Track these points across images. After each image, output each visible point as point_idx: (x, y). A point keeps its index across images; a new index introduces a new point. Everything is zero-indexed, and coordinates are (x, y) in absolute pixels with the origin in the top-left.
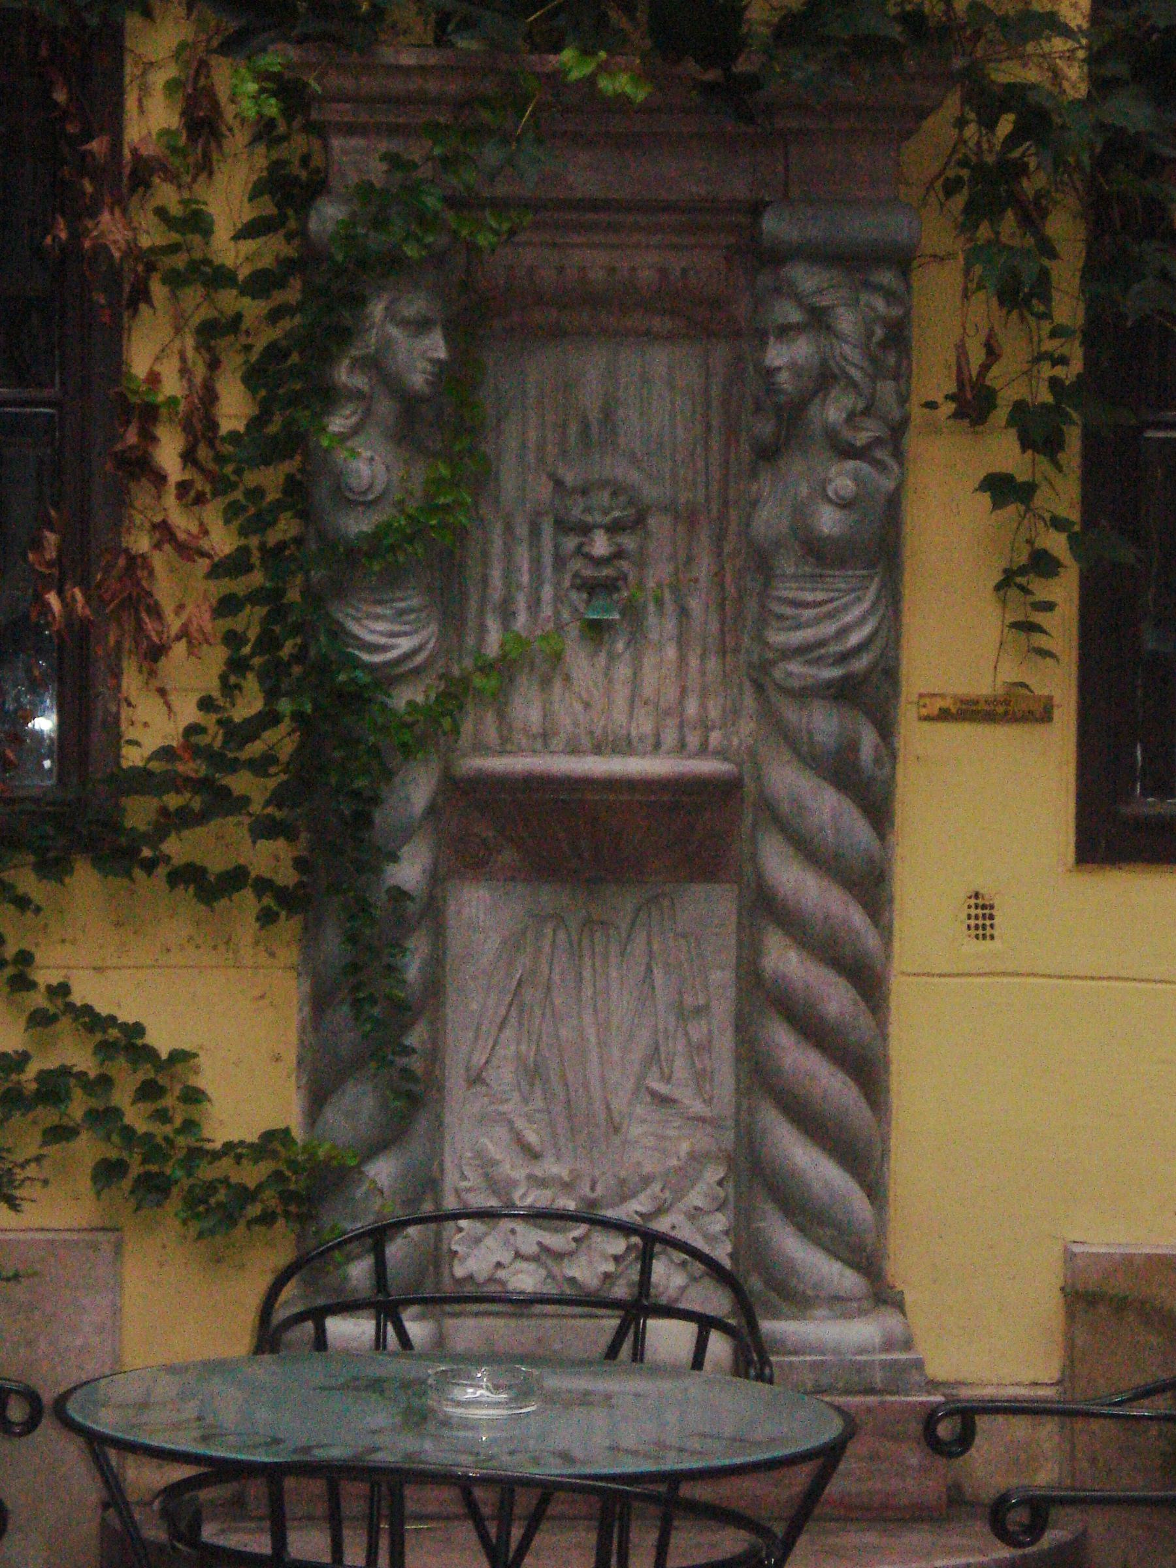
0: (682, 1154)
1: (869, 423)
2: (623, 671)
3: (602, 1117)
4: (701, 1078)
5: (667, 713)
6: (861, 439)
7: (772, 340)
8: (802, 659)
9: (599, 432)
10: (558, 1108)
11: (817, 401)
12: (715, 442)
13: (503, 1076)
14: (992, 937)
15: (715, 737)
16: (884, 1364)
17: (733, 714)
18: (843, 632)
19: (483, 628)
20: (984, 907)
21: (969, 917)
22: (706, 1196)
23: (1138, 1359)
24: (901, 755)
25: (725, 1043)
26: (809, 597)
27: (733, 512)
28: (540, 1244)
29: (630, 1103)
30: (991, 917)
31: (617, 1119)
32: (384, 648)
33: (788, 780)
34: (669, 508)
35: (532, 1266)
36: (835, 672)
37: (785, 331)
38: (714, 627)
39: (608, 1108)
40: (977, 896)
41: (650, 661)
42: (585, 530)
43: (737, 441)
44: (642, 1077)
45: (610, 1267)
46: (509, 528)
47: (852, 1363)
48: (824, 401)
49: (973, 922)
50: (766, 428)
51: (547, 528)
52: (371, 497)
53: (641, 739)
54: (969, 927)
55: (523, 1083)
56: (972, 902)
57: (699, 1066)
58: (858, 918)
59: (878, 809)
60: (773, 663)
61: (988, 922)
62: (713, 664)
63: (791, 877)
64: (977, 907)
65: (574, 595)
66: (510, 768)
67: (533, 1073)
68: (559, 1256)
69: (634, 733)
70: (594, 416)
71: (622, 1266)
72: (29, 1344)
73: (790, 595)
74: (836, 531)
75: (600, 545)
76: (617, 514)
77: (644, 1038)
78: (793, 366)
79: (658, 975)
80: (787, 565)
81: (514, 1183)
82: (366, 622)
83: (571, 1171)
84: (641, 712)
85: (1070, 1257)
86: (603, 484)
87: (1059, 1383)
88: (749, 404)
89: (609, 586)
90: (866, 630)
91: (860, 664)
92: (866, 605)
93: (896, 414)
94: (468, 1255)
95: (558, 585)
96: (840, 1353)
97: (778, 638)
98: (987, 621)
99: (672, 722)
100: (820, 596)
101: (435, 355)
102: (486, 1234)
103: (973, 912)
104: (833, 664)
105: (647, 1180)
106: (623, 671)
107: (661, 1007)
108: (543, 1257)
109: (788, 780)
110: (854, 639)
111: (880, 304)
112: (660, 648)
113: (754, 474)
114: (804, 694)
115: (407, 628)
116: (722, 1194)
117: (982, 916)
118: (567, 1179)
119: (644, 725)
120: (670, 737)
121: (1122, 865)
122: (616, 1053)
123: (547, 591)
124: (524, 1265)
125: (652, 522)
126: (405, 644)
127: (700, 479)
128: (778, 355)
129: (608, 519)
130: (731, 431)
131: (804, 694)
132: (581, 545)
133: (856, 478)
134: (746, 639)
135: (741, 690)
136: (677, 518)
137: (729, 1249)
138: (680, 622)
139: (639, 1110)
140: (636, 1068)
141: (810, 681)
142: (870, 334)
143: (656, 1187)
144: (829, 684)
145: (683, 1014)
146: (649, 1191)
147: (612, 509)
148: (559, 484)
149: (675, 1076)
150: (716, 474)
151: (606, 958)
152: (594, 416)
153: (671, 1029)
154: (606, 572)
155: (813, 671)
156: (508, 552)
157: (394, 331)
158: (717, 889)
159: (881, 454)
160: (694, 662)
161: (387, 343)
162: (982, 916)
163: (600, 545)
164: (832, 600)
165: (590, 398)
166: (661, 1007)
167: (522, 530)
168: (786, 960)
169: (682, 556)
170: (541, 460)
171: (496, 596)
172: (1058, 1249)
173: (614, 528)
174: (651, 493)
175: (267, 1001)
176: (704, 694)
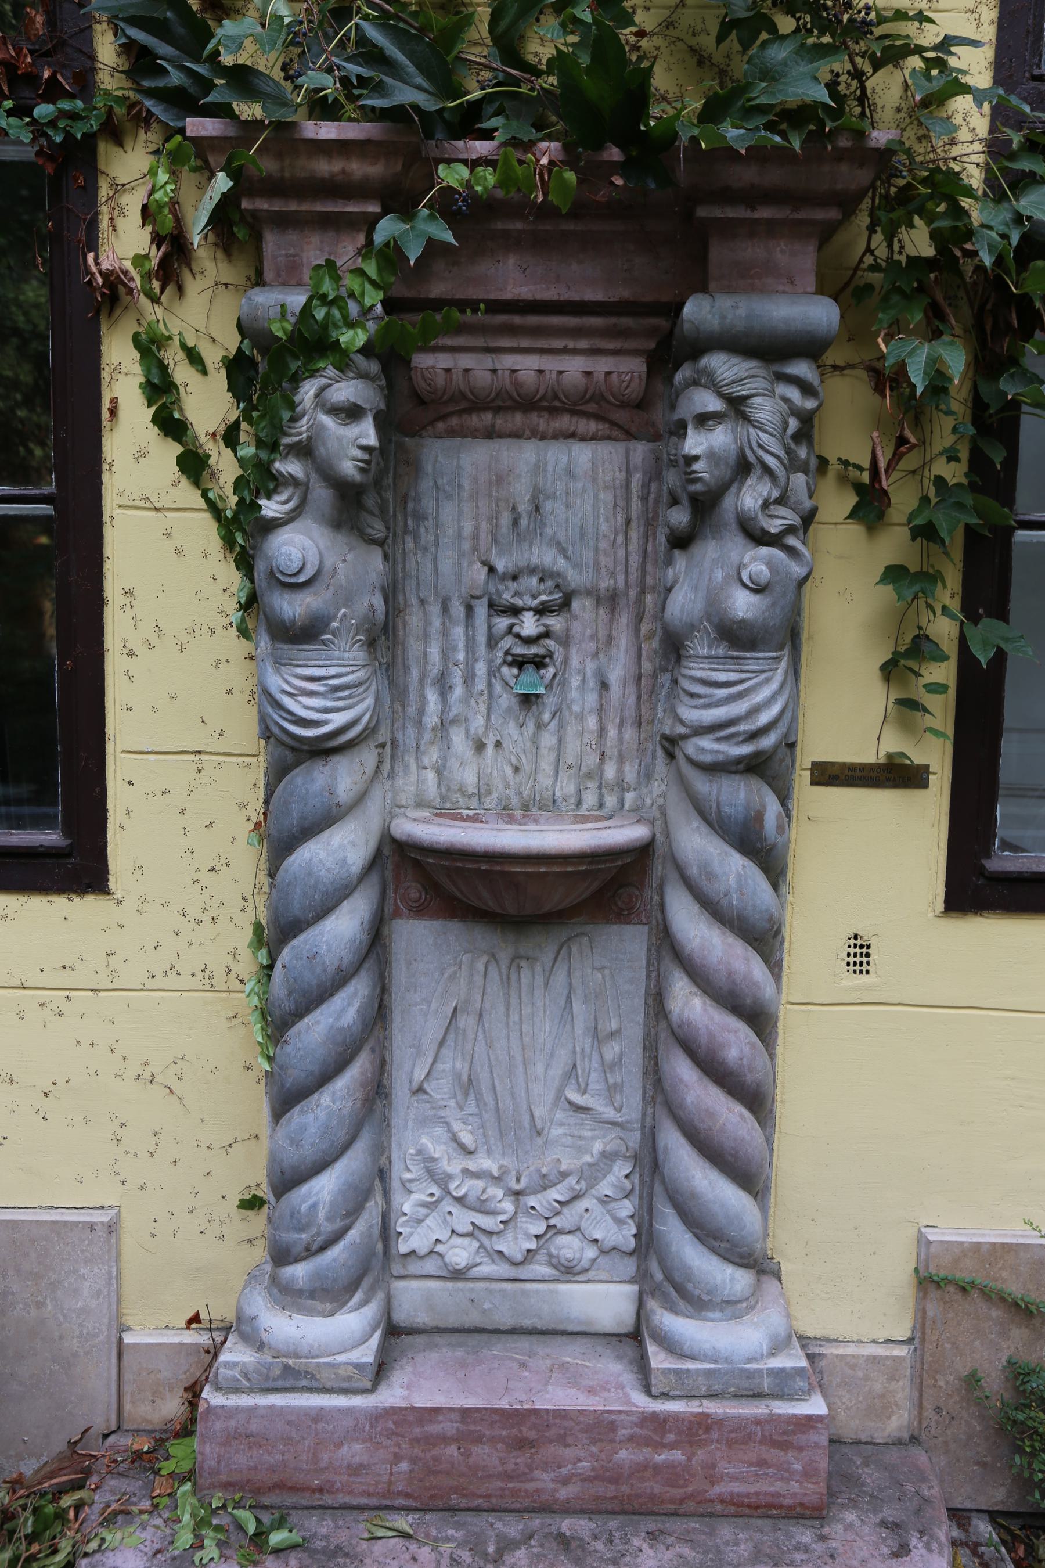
0: (595, 1151)
1: (782, 511)
2: (548, 739)
3: (526, 1123)
4: (612, 1090)
5: (589, 776)
6: (774, 526)
7: (690, 431)
8: (711, 736)
9: (528, 520)
10: (489, 1117)
11: (735, 485)
12: (634, 535)
13: (441, 1089)
14: (868, 972)
15: (630, 797)
16: (772, 1372)
17: (647, 775)
18: (755, 710)
19: (423, 697)
20: (862, 946)
21: (849, 955)
22: (615, 1186)
23: (989, 1350)
24: (794, 813)
25: (635, 1059)
26: (722, 677)
27: (649, 598)
28: (473, 1223)
29: (551, 1109)
30: (868, 955)
31: (539, 1124)
32: (325, 722)
33: (697, 844)
34: (591, 592)
35: (466, 1241)
36: (746, 749)
37: (703, 420)
38: (632, 700)
39: (532, 1115)
40: (856, 937)
41: (572, 729)
42: (515, 611)
43: (654, 534)
44: (560, 1092)
45: (533, 1245)
46: (445, 608)
47: (742, 1370)
48: (739, 490)
49: (851, 960)
50: (680, 517)
51: (481, 610)
52: (302, 579)
53: (565, 800)
54: (848, 964)
55: (458, 1093)
56: (852, 942)
57: (611, 1081)
58: (758, 970)
59: (771, 862)
60: (684, 737)
61: (865, 959)
62: (629, 733)
63: (693, 928)
64: (855, 946)
65: (505, 670)
66: (435, 838)
67: (468, 1086)
68: (490, 1233)
69: (558, 794)
70: (524, 508)
71: (541, 1242)
72: (39, 1305)
73: (699, 674)
74: (749, 616)
75: (529, 625)
76: (544, 598)
77: (563, 1057)
78: (712, 455)
79: (577, 1006)
80: (699, 646)
81: (450, 1177)
82: (300, 698)
83: (501, 1167)
84: (564, 775)
85: (922, 1241)
86: (532, 570)
87: (910, 1341)
88: (665, 497)
89: (538, 663)
90: (775, 710)
91: (768, 742)
92: (774, 686)
93: (808, 504)
94: (411, 1234)
95: (490, 662)
96: (732, 1362)
97: (692, 714)
98: (875, 699)
99: (592, 785)
100: (733, 677)
101: (364, 442)
102: (427, 1216)
103: (852, 951)
104: (744, 741)
105: (564, 1175)
106: (548, 739)
107: (579, 1030)
108: (477, 1232)
109: (697, 844)
110: (764, 718)
111: (794, 394)
112: (581, 718)
113: (669, 562)
114: (715, 769)
115: (341, 704)
116: (629, 1186)
117: (860, 954)
118: (496, 1174)
119: (566, 787)
120: (590, 799)
121: (985, 914)
122: (540, 1069)
123: (481, 668)
124: (459, 1241)
125: (575, 605)
126: (338, 719)
127: (620, 568)
128: (695, 443)
129: (536, 602)
130: (649, 524)
131: (715, 769)
132: (511, 627)
133: (769, 564)
134: (660, 710)
135: (654, 756)
136: (598, 601)
137: (634, 1231)
138: (601, 696)
139: (559, 1115)
140: (557, 1082)
141: (721, 757)
142: (785, 425)
143: (572, 1180)
144: (739, 760)
145: (599, 1037)
146: (565, 1183)
147: (540, 594)
148: (492, 570)
149: (591, 1086)
150: (635, 561)
151: (532, 986)
152: (524, 508)
153: (588, 1050)
154: (533, 650)
155: (722, 747)
156: (445, 633)
157: (327, 421)
158: (629, 930)
159: (791, 541)
160: (612, 733)
161: (317, 430)
162: (860, 954)
163: (529, 625)
164: (742, 681)
165: (521, 491)
166: (579, 1030)
167: (458, 610)
168: (689, 1004)
169: (602, 634)
170: (475, 548)
171: (434, 671)
172: (913, 1232)
173: (541, 611)
174: (574, 578)
175: (239, 1020)
176: (621, 759)
